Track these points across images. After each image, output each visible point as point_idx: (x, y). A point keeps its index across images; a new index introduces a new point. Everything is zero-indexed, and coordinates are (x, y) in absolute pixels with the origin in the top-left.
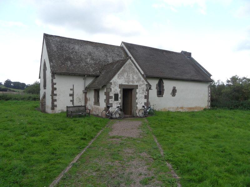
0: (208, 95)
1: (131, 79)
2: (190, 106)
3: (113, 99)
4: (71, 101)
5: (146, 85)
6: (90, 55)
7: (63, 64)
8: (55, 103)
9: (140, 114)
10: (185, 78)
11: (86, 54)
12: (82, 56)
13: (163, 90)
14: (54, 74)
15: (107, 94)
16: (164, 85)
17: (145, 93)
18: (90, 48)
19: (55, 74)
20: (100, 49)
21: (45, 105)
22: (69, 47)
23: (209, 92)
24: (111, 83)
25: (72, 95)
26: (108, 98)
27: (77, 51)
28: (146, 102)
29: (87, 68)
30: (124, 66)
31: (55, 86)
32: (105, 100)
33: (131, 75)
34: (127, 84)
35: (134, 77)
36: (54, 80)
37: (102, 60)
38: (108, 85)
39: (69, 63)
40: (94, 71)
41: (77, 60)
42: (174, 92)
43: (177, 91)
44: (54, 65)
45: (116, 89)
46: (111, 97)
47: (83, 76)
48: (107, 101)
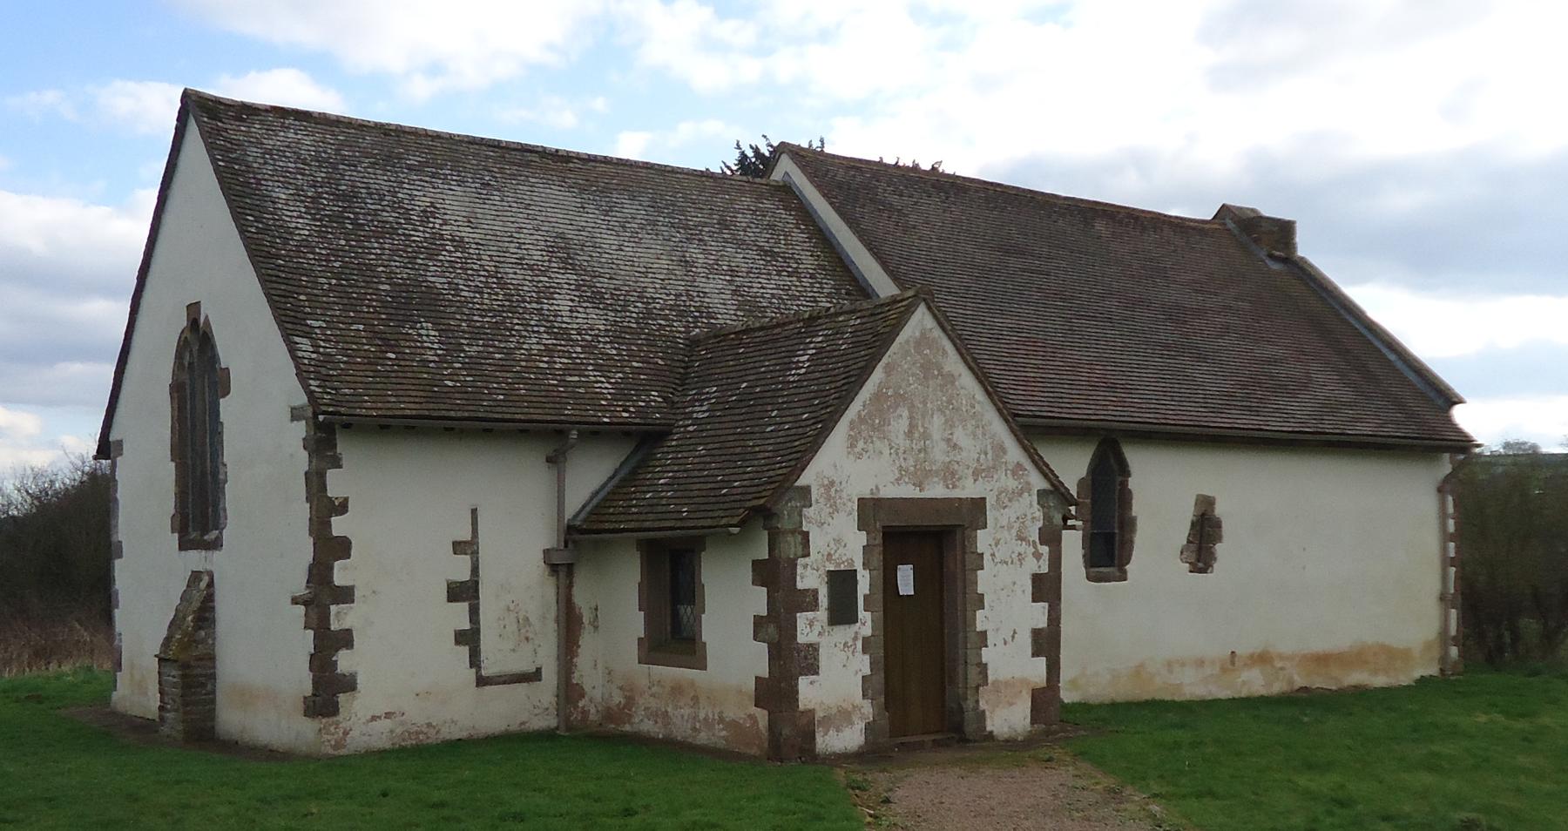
0: (1444, 549)
1: (939, 454)
2: (1319, 645)
3: (822, 614)
4: (461, 637)
5: (1041, 493)
6: (568, 263)
7: (388, 344)
8: (345, 661)
9: (1008, 717)
10: (1275, 424)
11: (537, 255)
12: (514, 276)
13: (1128, 525)
14: (328, 431)
15: (774, 575)
16: (1133, 483)
17: (1037, 556)
18: (557, 206)
19: (347, 426)
20: (630, 208)
21: (213, 677)
22: (396, 206)
23: (1444, 525)
24: (806, 490)
25: (464, 592)
26: (784, 600)
27: (466, 233)
28: (1042, 623)
29: (567, 370)
30: (885, 360)
31: (339, 526)
32: (759, 622)
33: (936, 424)
34: (908, 491)
35: (960, 436)
36: (332, 475)
37: (663, 299)
38: (786, 507)
39: (428, 332)
40: (621, 393)
41: (483, 313)
42: (1204, 537)
43: (1227, 529)
44: (328, 360)
45: (834, 540)
46: (808, 601)
47: (550, 435)
48: (776, 628)
